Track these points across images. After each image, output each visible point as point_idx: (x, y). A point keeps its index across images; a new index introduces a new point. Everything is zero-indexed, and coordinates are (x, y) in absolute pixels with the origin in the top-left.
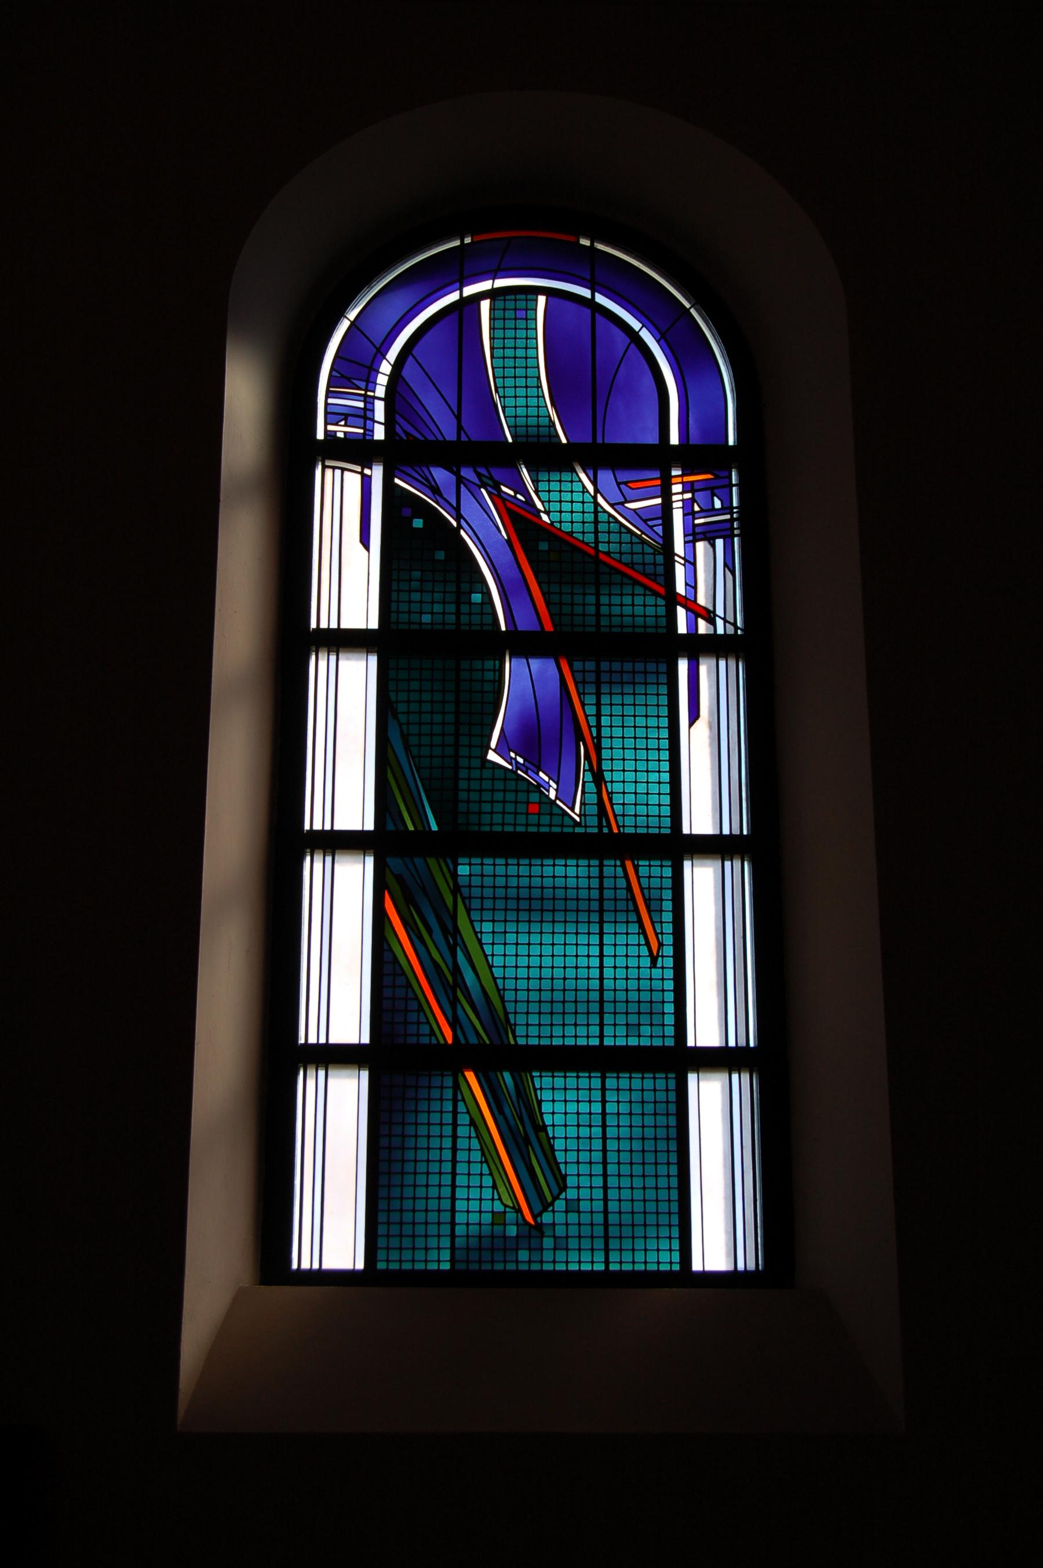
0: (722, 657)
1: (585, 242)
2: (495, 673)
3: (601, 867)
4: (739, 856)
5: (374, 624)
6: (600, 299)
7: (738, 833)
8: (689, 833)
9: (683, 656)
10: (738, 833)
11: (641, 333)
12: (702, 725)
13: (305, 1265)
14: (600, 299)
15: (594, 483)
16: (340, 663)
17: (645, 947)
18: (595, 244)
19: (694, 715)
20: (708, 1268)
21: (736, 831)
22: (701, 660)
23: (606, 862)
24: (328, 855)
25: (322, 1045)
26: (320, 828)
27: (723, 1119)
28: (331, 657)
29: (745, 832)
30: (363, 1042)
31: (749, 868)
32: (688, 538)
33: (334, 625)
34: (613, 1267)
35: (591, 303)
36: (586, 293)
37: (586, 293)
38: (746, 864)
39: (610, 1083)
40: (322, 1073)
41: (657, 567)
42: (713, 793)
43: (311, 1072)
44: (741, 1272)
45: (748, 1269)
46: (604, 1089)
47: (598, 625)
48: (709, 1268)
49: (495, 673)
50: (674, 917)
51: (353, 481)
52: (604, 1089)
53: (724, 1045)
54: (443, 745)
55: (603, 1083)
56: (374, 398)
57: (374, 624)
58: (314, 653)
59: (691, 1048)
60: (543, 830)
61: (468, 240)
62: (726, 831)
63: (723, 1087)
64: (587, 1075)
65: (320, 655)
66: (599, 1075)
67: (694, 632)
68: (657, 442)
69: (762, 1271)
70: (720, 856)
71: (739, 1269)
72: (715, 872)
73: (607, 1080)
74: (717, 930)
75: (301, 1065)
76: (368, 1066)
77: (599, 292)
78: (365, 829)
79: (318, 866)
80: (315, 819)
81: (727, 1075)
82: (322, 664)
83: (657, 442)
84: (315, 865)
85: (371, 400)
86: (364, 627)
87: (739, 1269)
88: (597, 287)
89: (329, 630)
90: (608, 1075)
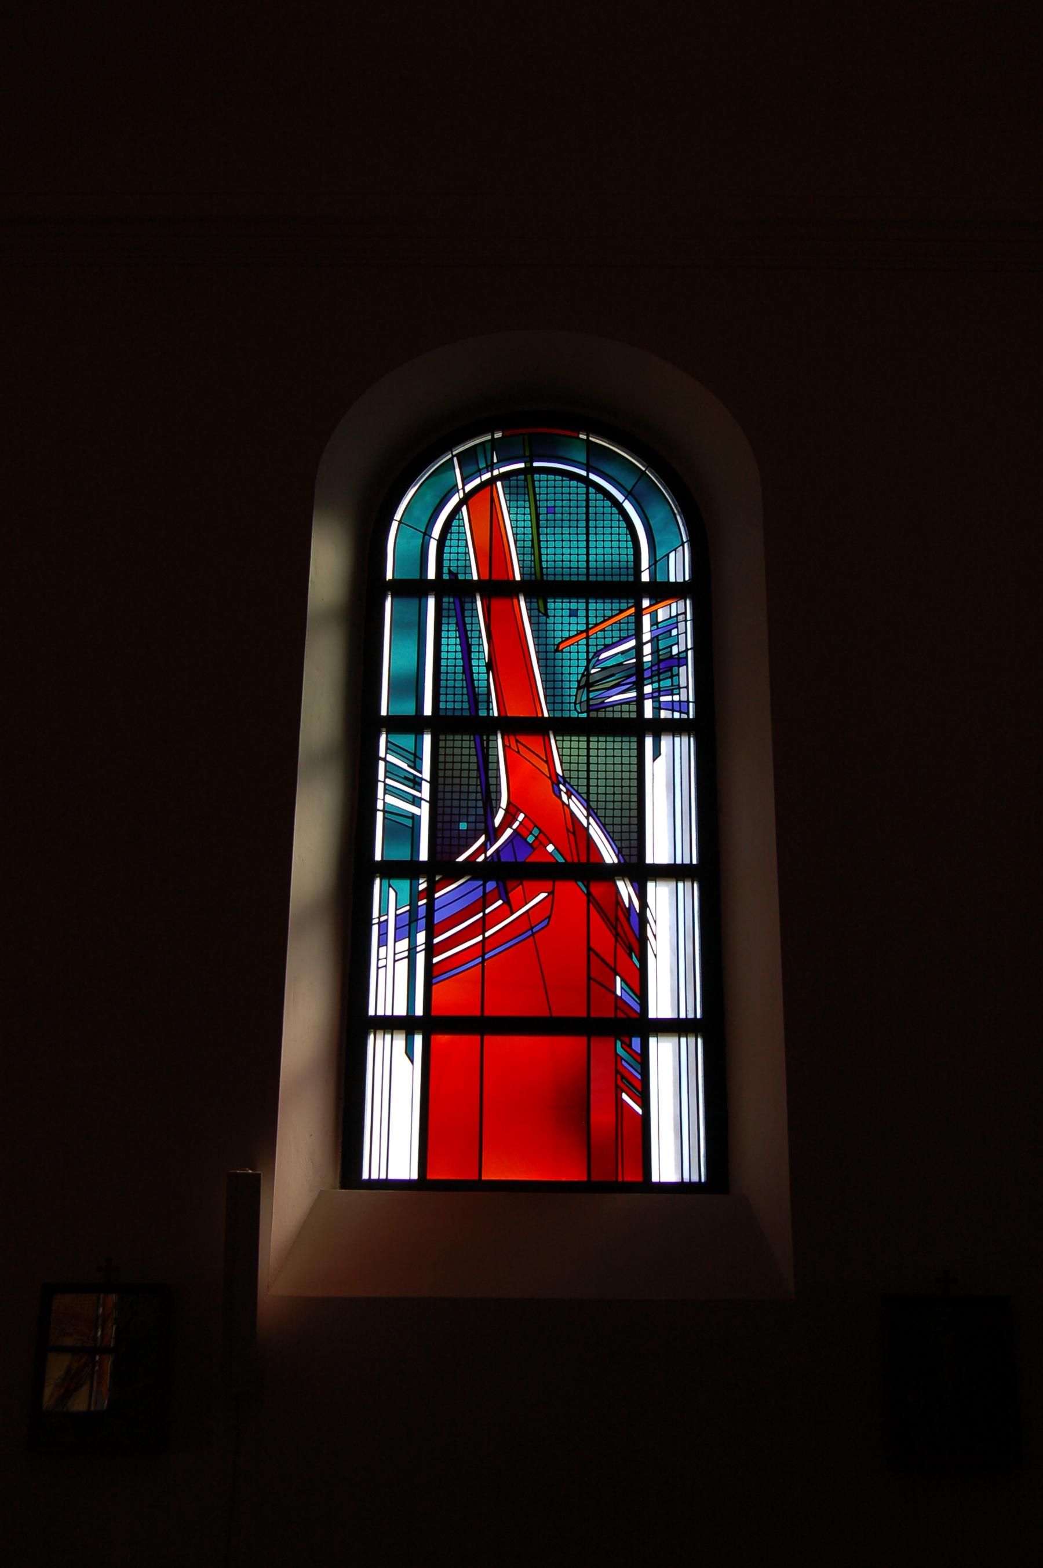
0: (680, 880)
1: (583, 436)
3: (588, 741)
4: (687, 734)
5: (415, 1176)
6: (592, 477)
9: (646, 597)
11: (624, 505)
12: (661, 759)
14: (592, 477)
15: (587, 888)
16: (394, 1042)
17: (615, 707)
20: (662, 1180)
22: (662, 738)
23: (591, 739)
27: (676, 1165)
29: (699, 1016)
32: (653, 628)
36: (584, 473)
38: (688, 602)
39: (592, 606)
41: (629, 570)
42: (674, 1069)
43: (380, 1036)
44: (686, 1183)
46: (587, 610)
47: (587, 603)
48: (660, 1016)
50: (634, 552)
51: (400, 1042)
52: (587, 610)
55: (587, 606)
56: (421, 799)
57: (415, 1176)
59: (656, 1183)
61: (498, 435)
62: (683, 1015)
63: (670, 892)
64: (576, 601)
66: (584, 601)
67: (658, 717)
69: (704, 1182)
70: (671, 733)
71: (685, 1180)
72: (673, 1045)
73: (590, 605)
74: (674, 1087)
75: (372, 1030)
76: (434, 593)
77: (592, 473)
82: (379, 1042)
85: (419, 780)
87: (685, 1180)
88: (591, 468)
90: (590, 601)
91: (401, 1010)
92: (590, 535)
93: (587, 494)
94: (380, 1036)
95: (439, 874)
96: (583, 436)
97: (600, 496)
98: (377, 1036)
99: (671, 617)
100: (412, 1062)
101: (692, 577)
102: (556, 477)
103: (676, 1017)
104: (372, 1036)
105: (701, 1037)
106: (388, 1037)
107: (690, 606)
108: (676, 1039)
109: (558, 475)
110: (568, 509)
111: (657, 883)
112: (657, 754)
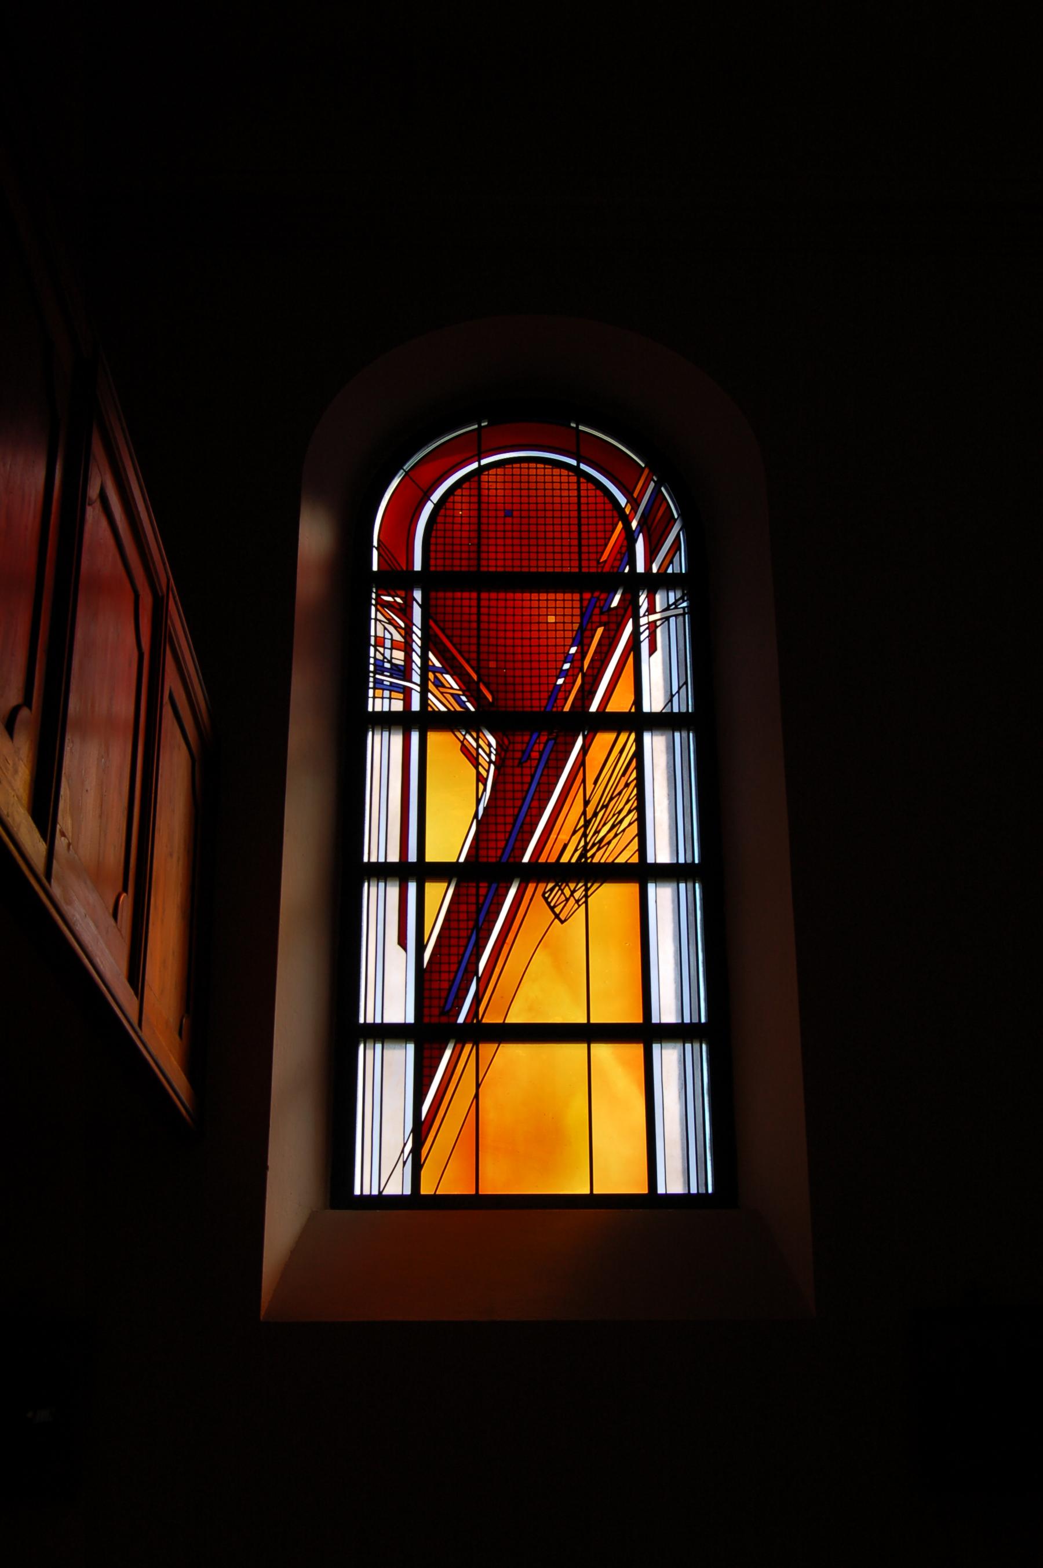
0: (671, 590)
1: (573, 425)
2: (502, 566)
3: (580, 567)
5: (411, 1019)
6: (583, 467)
7: (679, 572)
8: (664, 1192)
10: (679, 572)
12: (658, 655)
13: (370, 1020)
14: (583, 467)
18: (580, 426)
19: (653, 649)
21: (683, 710)
24: (382, 882)
25: (382, 863)
26: (372, 1022)
28: (380, 884)
29: (684, 571)
30: (408, 1021)
31: (699, 888)
33: (382, 860)
34: (584, 570)
35: (576, 470)
36: (574, 462)
37: (574, 462)
38: (697, 885)
40: (379, 1046)
43: (373, 884)
45: (681, 711)
49: (502, 566)
51: (397, 740)
53: (687, 1192)
54: (469, 559)
57: (411, 1019)
58: (371, 729)
59: (662, 1195)
60: (540, 570)
62: (687, 1020)
65: (371, 884)
68: (646, 1192)
78: (404, 1193)
79: (377, 738)
80: (368, 1013)
81: (682, 1045)
82: (373, 890)
83: (646, 1192)
84: (367, 1051)
86: (402, 1021)
89: (374, 1025)
91: (394, 857)
92: (583, 562)
93: (578, 483)
94: (373, 884)
95: (427, 709)
96: (573, 425)
97: (591, 486)
98: (367, 1045)
99: (669, 606)
100: (405, 949)
101: (695, 708)
102: (544, 571)
103: (675, 862)
104: (370, 734)
105: (698, 883)
106: (386, 734)
107: (692, 699)
108: (675, 885)
109: (542, 573)
110: (559, 548)
111: (663, 1045)
112: (653, 649)
